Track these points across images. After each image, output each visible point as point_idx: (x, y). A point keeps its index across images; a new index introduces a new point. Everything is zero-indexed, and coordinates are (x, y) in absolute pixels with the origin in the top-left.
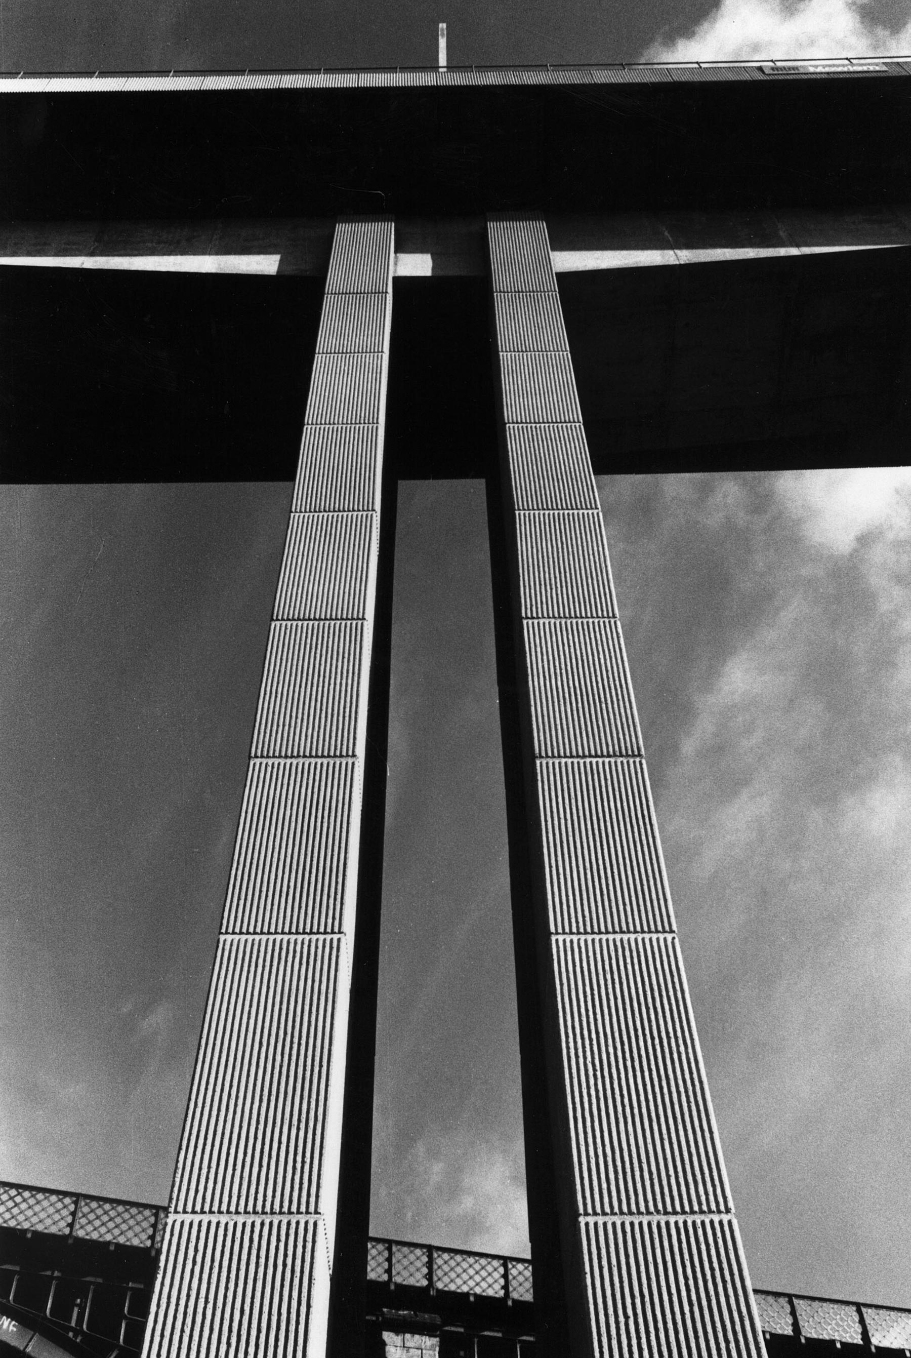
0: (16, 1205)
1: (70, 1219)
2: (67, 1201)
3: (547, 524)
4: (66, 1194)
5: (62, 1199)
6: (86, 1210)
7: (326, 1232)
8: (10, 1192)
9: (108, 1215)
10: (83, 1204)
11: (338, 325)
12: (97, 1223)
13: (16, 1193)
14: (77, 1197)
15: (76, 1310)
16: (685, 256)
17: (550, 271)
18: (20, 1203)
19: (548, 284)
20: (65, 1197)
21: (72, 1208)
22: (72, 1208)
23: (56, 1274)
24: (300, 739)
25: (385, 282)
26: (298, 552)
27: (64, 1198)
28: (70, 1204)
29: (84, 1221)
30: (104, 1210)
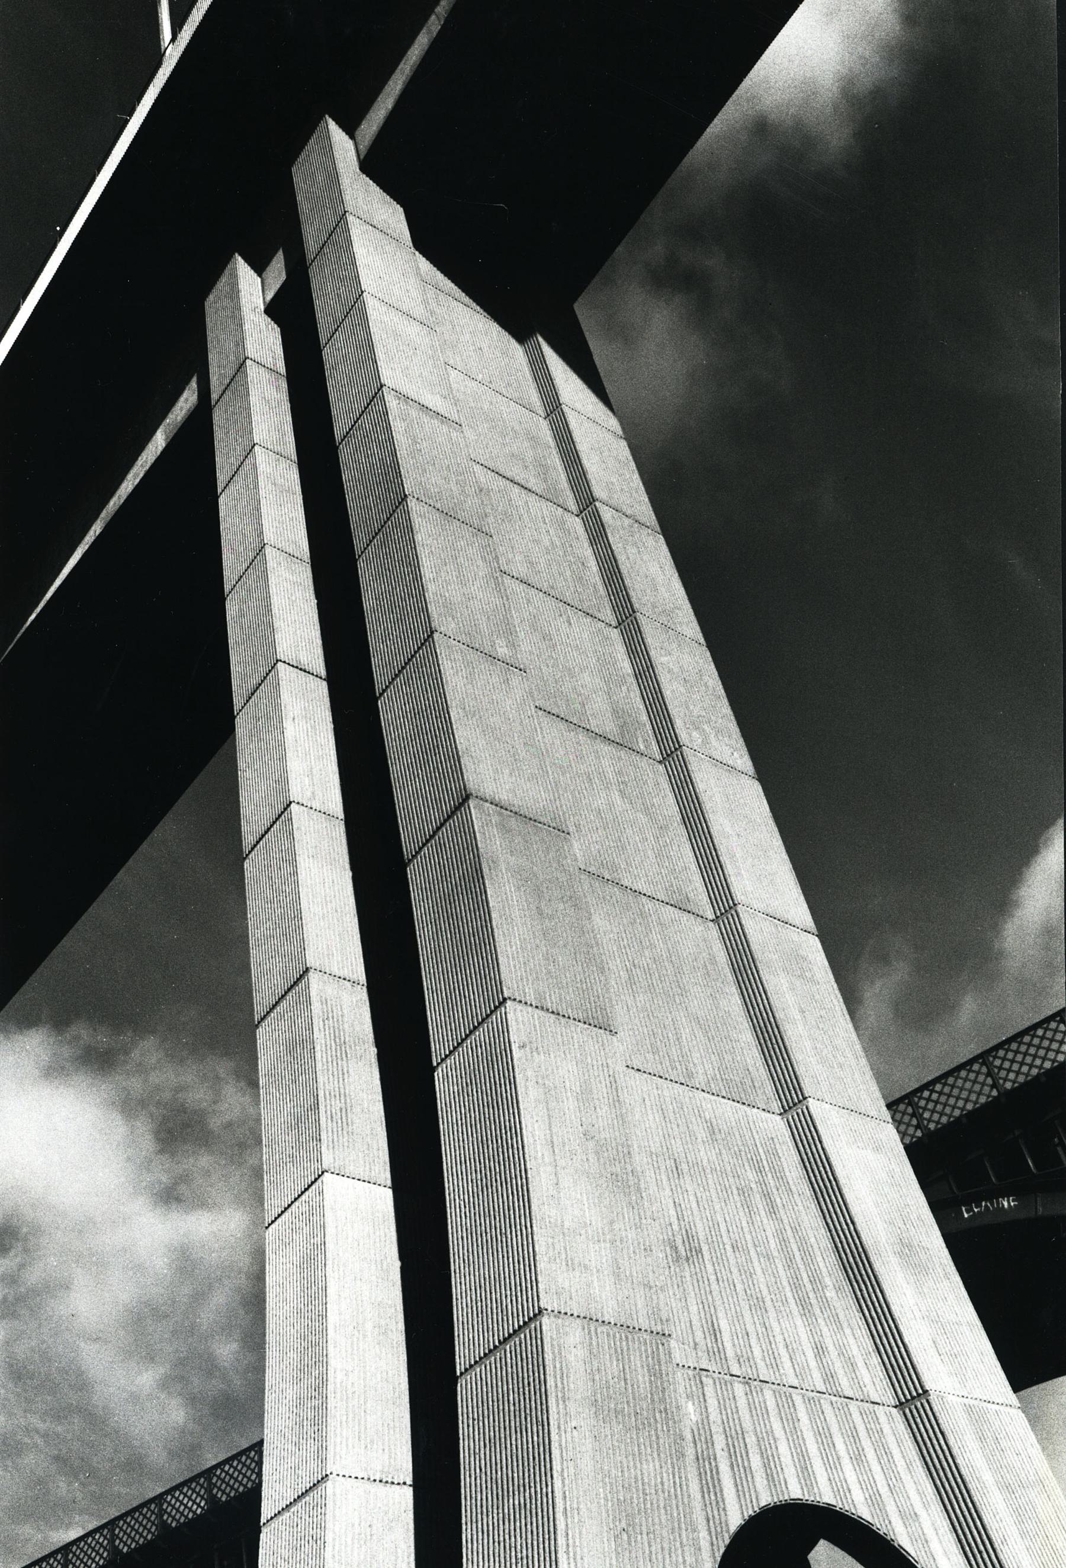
0: (937, 1102)
1: (989, 1081)
2: (976, 1067)
3: (943, 1460)
4: (971, 1062)
5: (1048, 1026)
6: (922, 1103)
7: (341, 1475)
8: (999, 1055)
9: (1020, 1053)
10: (991, 1059)
11: (735, 957)
12: (1015, 1067)
13: (1004, 1052)
14: (983, 1057)
15: (1059, 1149)
16: (396, 85)
17: (743, 937)
18: (1036, 1053)
19: (724, 898)
20: (997, 1052)
21: (910, 1110)
22: (984, 1070)
23: (1017, 1133)
24: (913, 1383)
25: (774, 1025)
26: (726, 897)
27: (1036, 1031)
28: (980, 1068)
29: (1003, 1074)
30: (924, 1099)
